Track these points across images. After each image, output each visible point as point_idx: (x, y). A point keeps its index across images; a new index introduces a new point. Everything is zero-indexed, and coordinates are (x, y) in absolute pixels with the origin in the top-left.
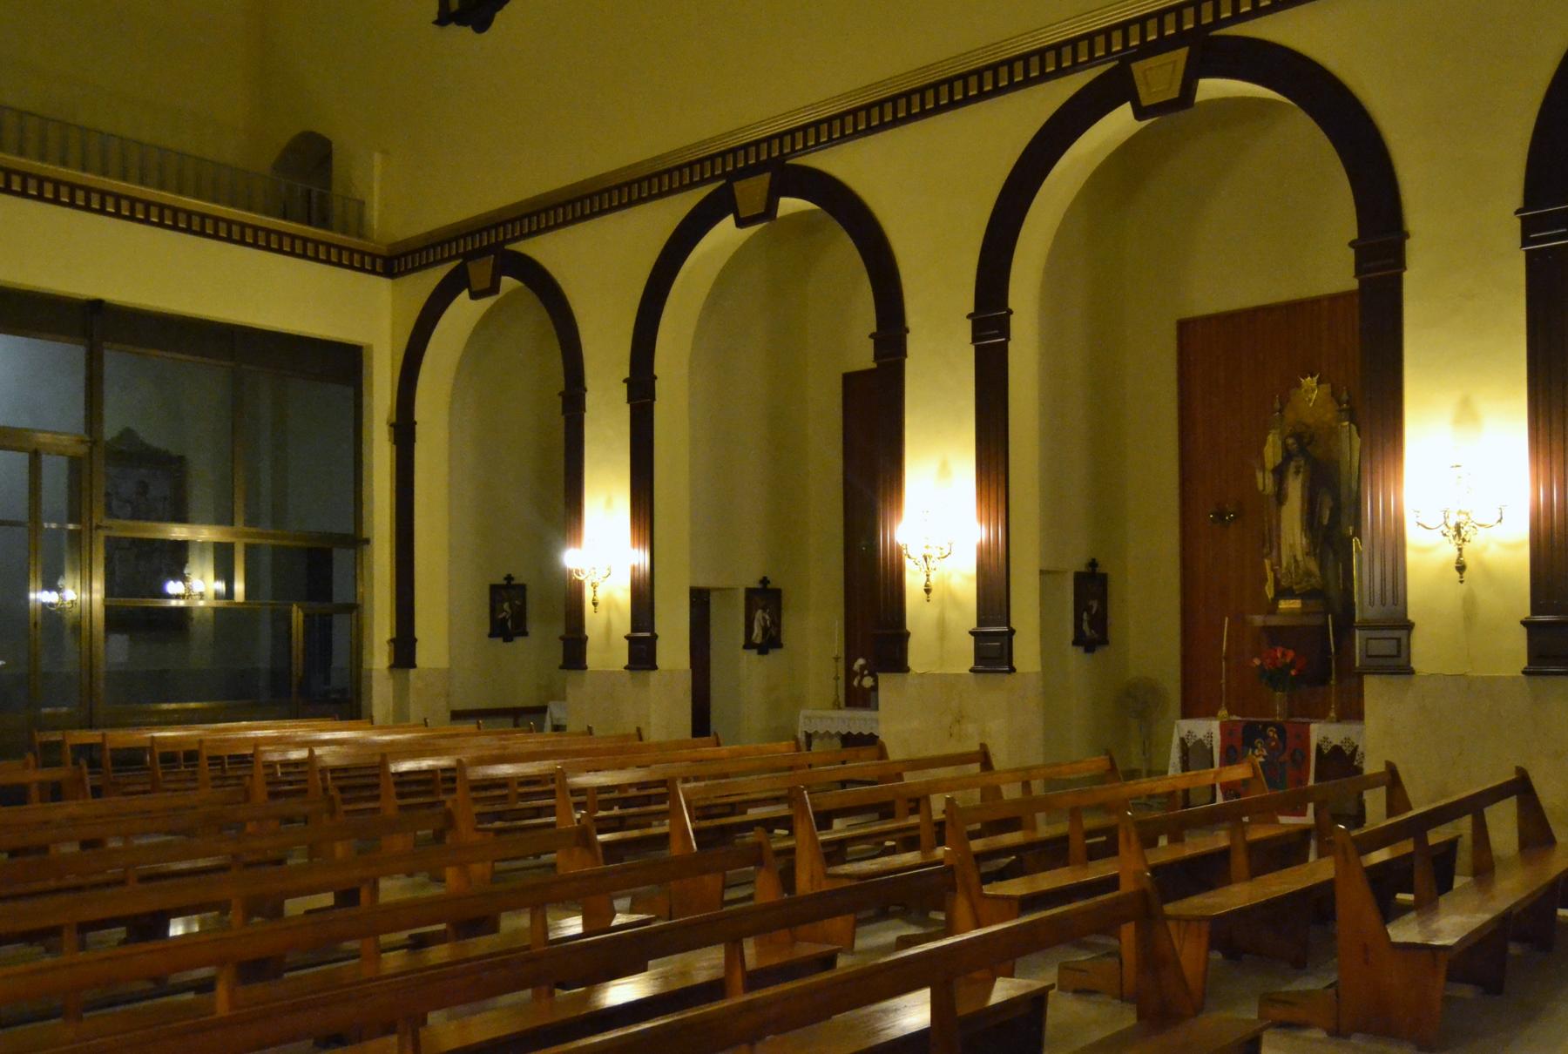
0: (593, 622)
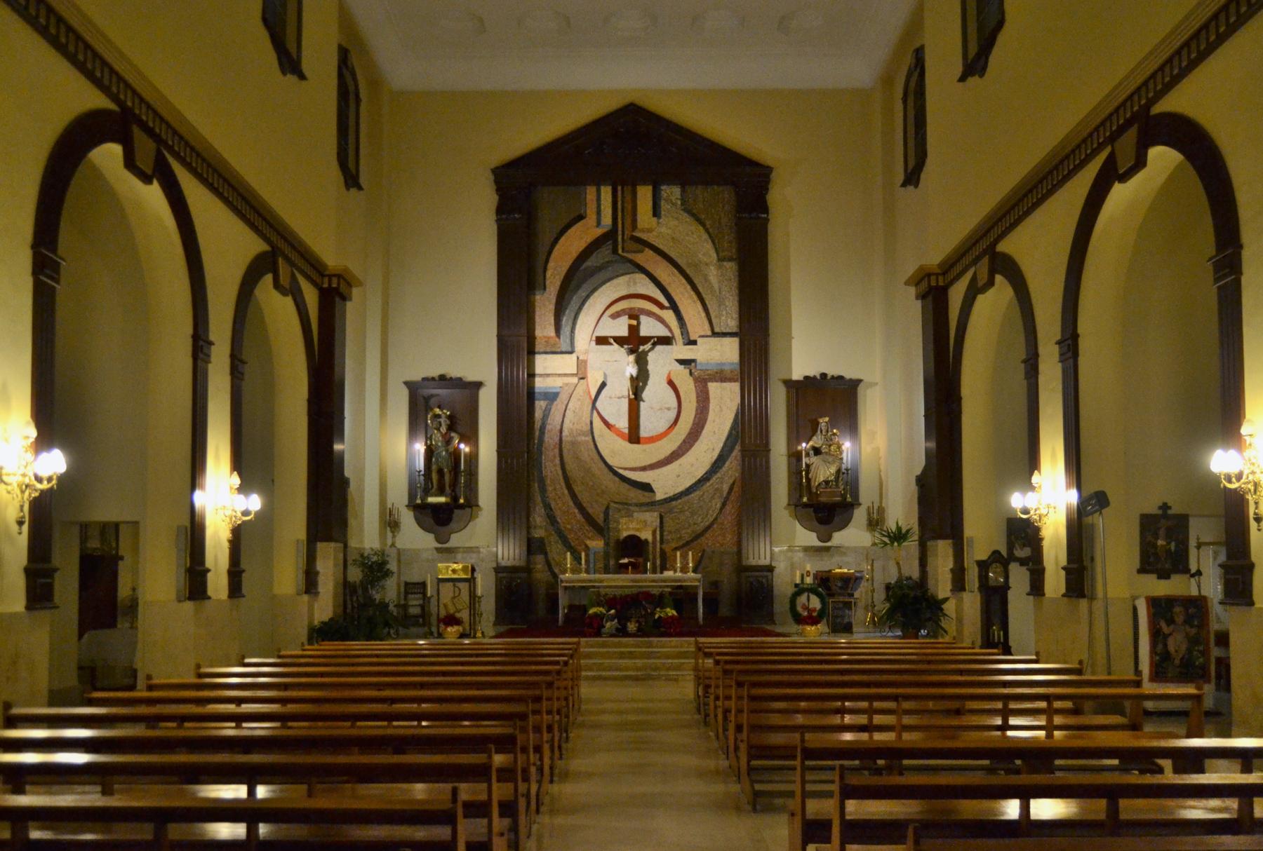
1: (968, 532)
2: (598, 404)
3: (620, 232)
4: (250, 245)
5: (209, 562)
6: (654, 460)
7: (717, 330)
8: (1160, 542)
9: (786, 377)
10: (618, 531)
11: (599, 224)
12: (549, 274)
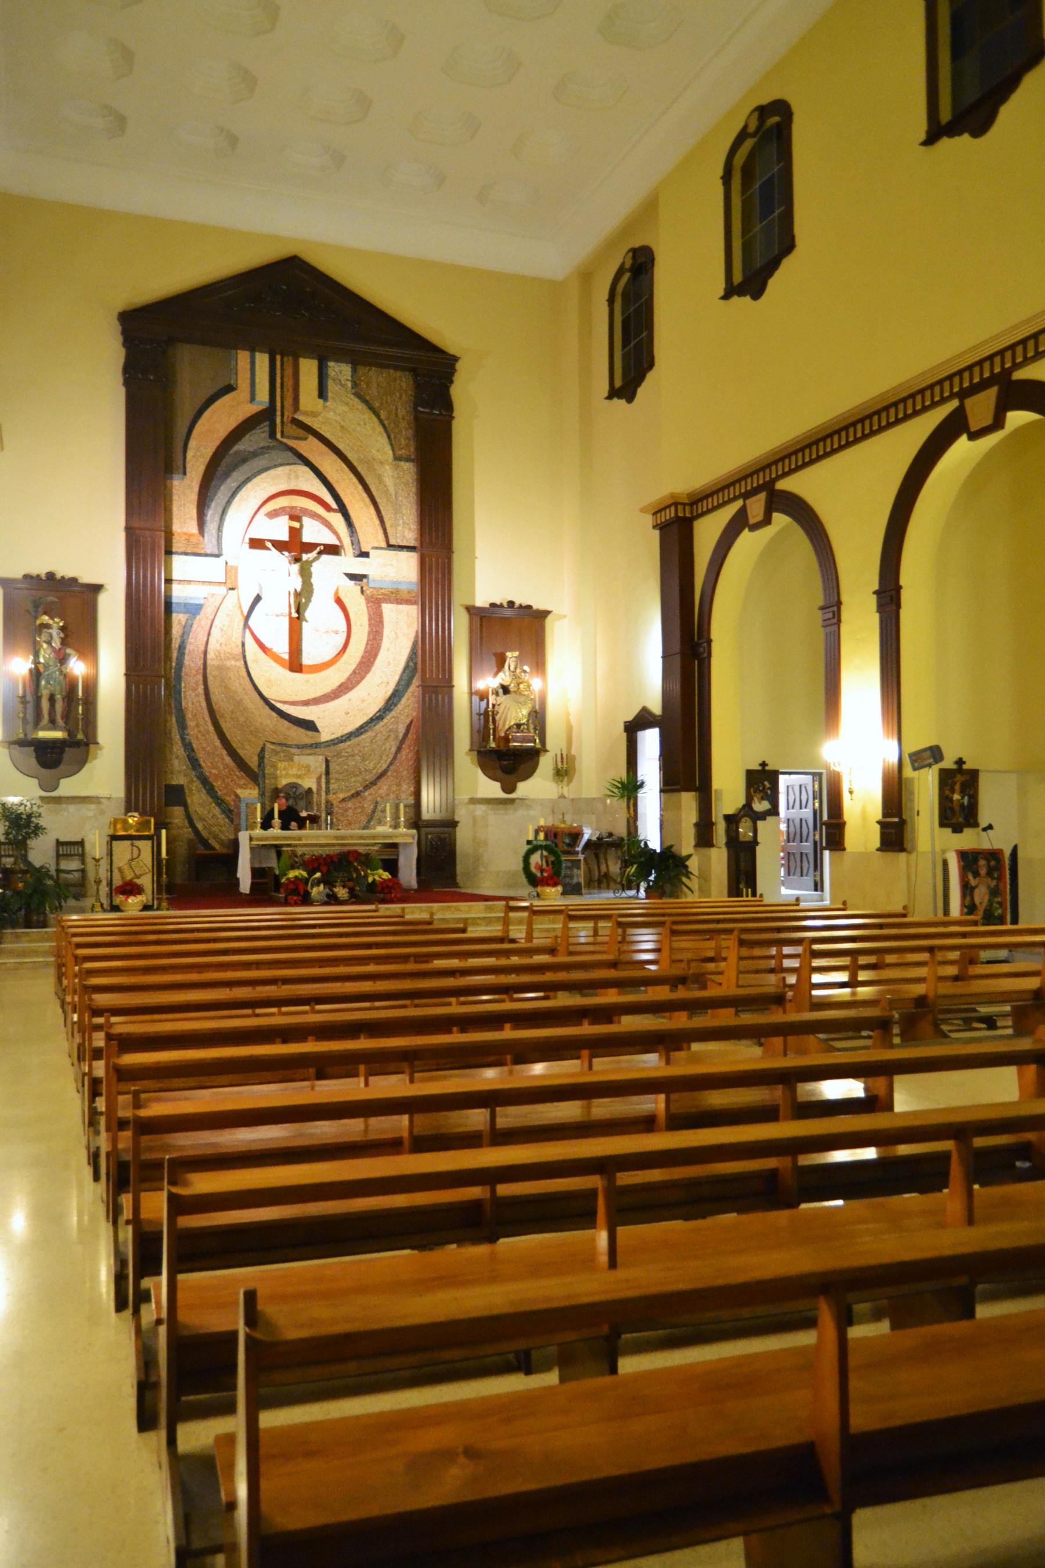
0: (851, 808)
1: (717, 784)
2: (251, 622)
3: (279, 413)
6: (319, 693)
7: (392, 542)
8: (956, 797)
9: (469, 603)
10: (276, 778)
11: (253, 398)
12: (190, 454)
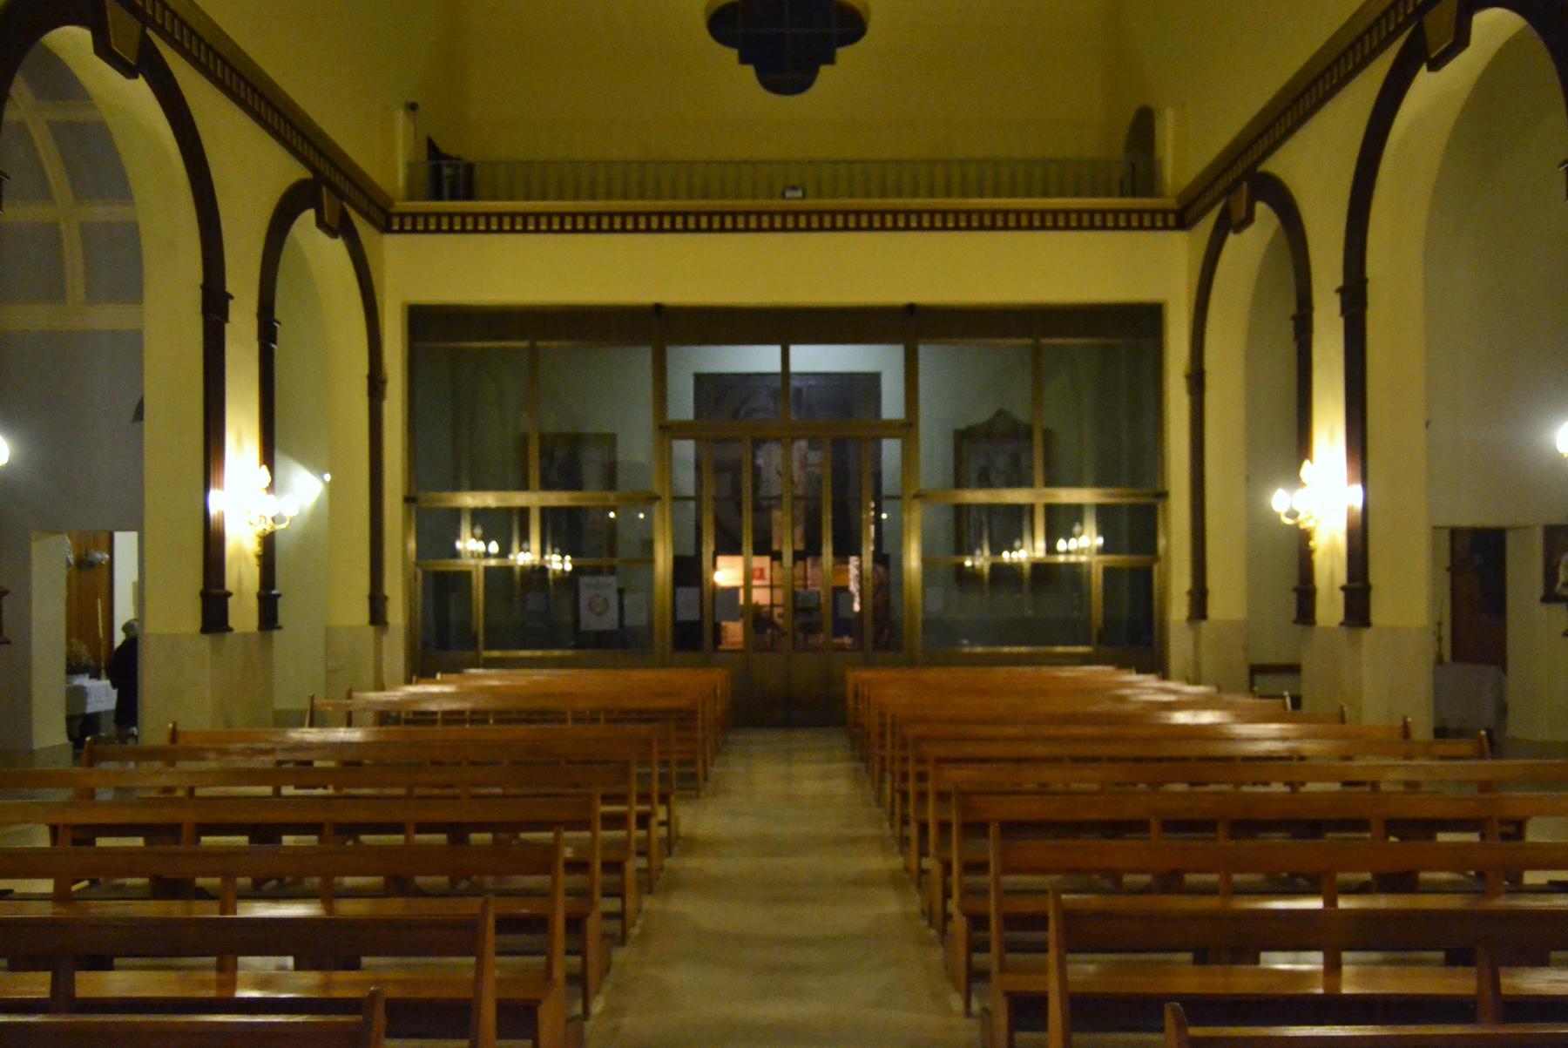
4: (284, 170)
5: (230, 583)
